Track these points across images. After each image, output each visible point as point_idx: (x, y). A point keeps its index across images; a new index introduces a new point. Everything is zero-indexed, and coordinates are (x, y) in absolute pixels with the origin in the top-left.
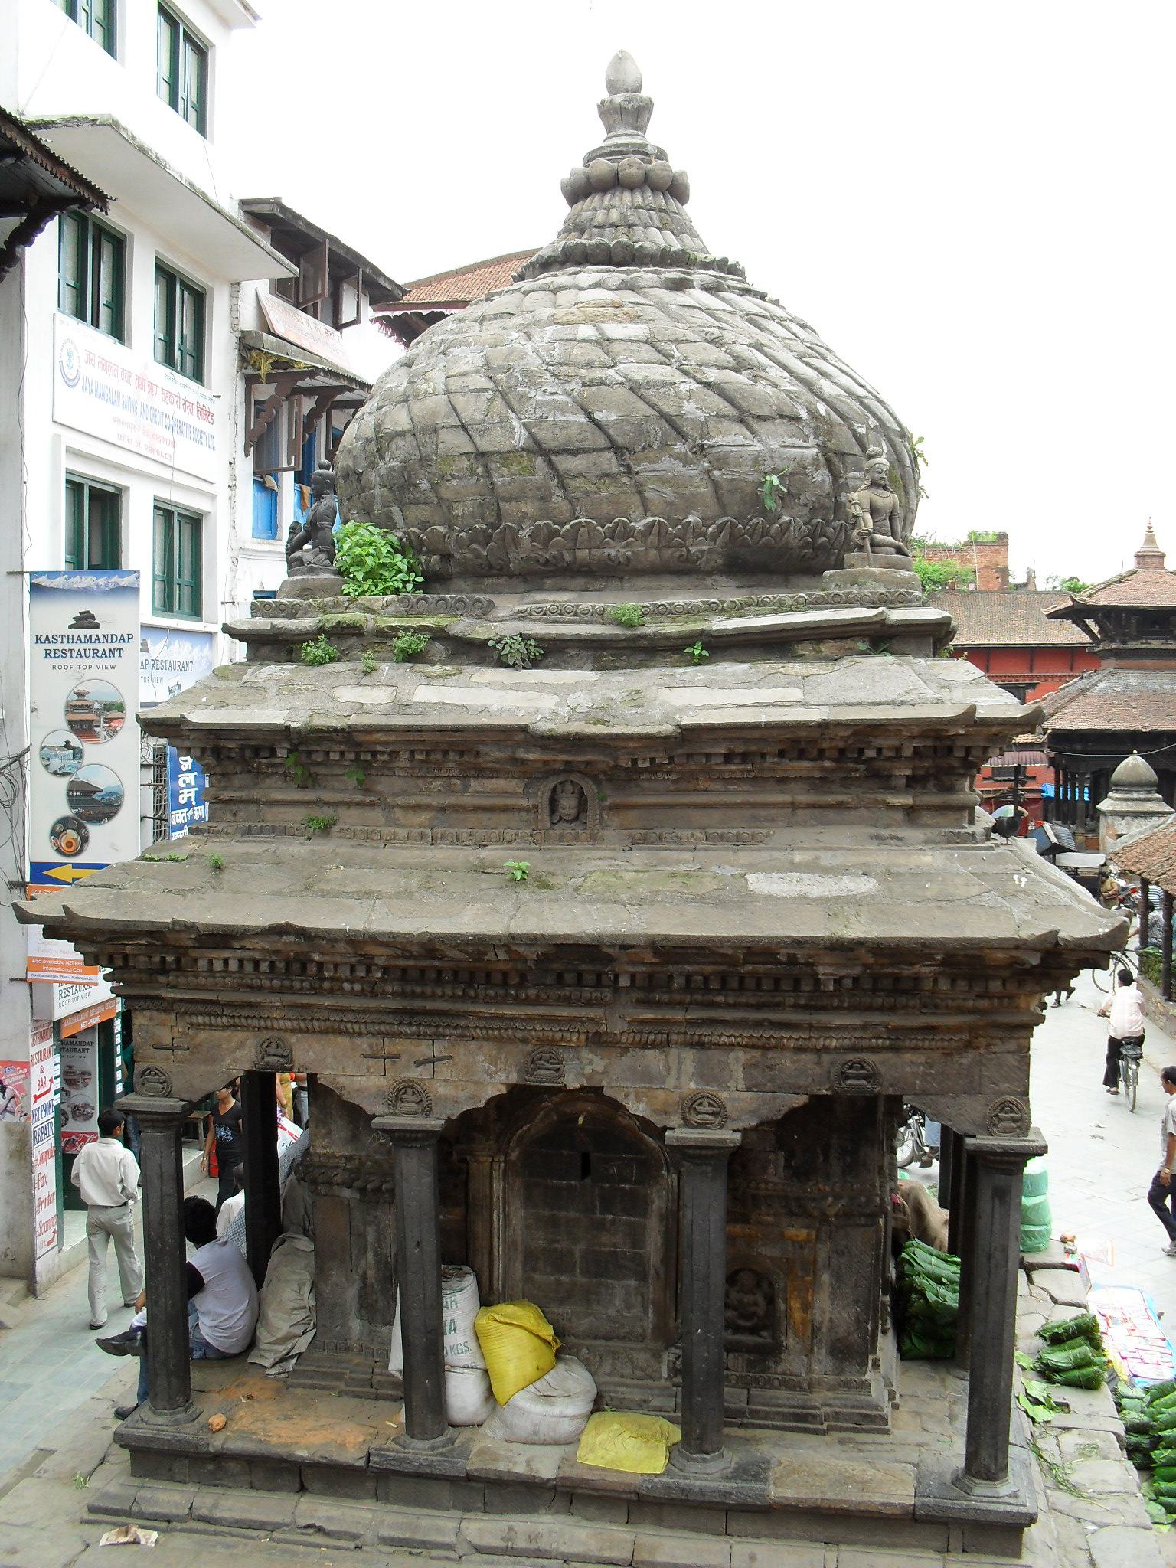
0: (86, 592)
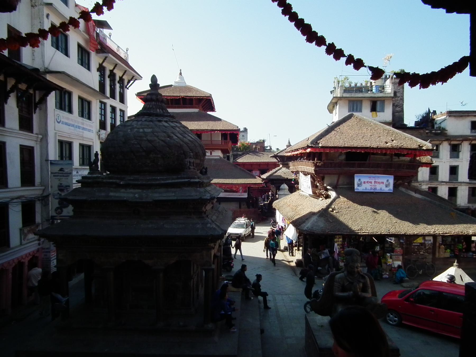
0: (62, 164)
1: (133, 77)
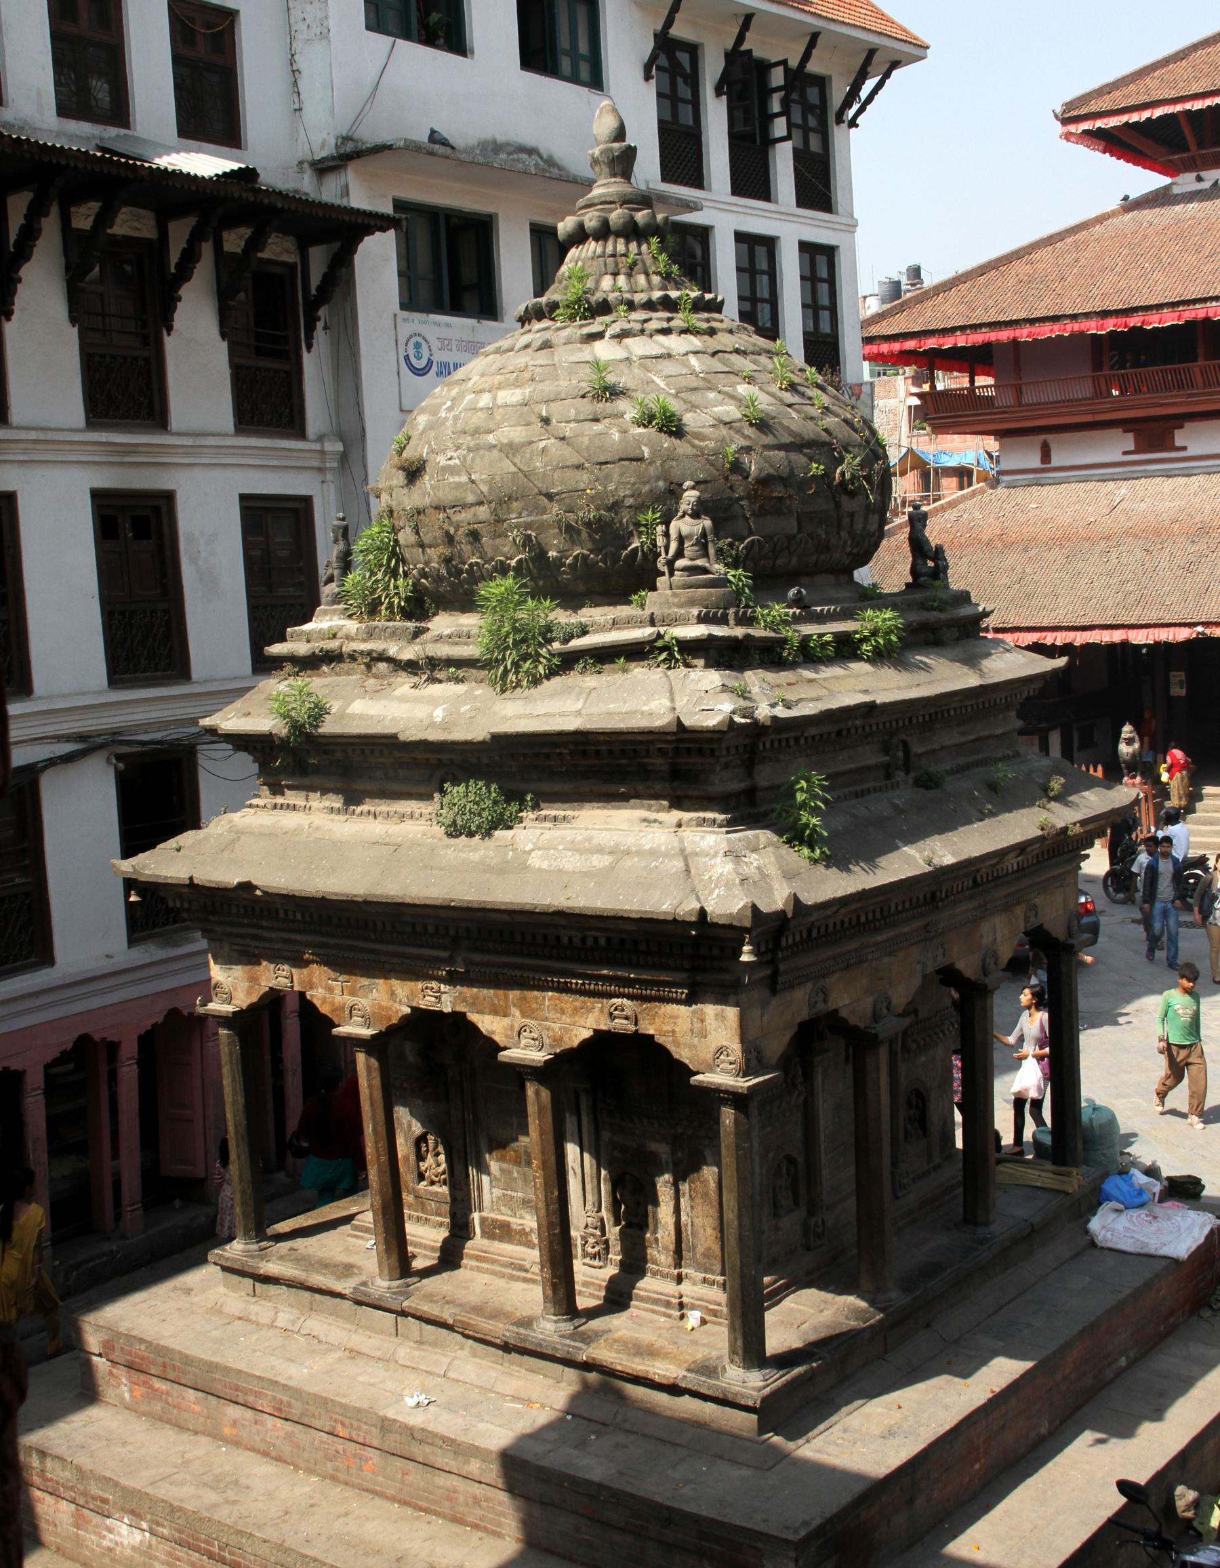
1: (872, 52)
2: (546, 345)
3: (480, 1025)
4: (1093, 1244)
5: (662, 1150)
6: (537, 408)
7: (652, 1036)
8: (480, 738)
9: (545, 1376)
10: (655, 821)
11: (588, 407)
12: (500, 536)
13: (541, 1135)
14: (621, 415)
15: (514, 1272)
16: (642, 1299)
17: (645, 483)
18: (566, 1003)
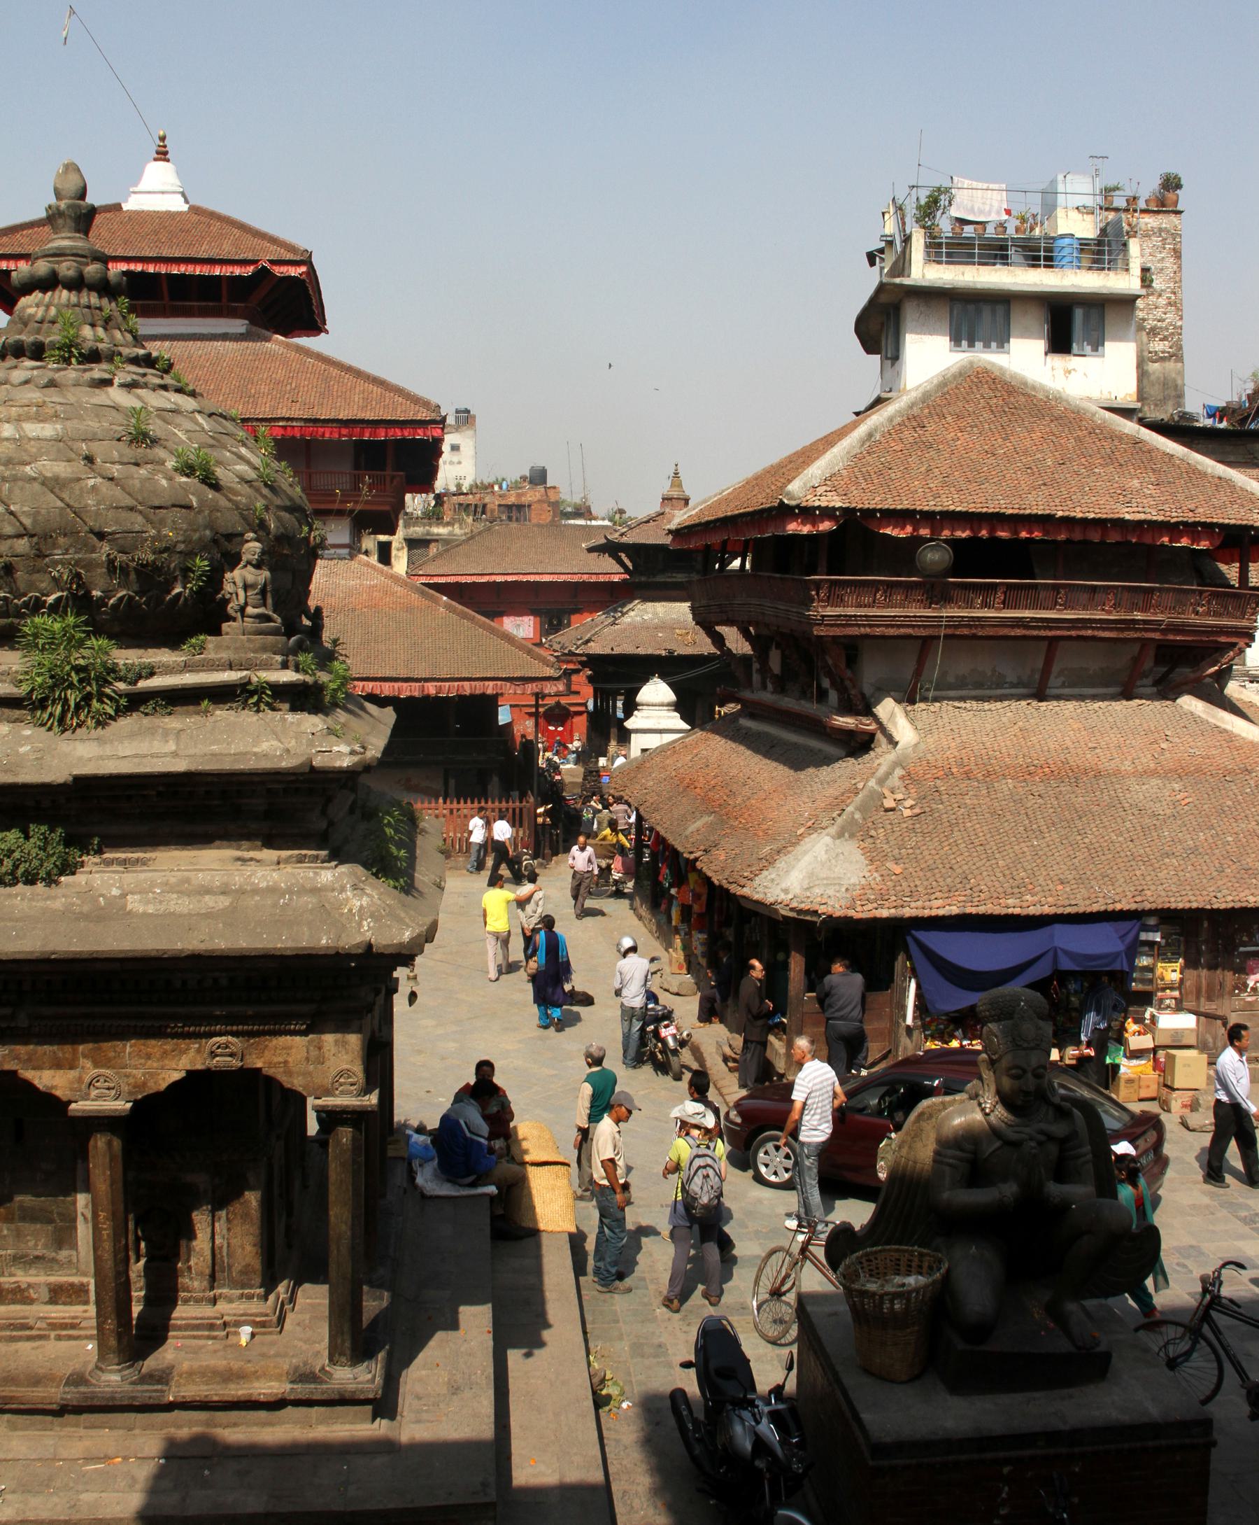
2: (52, 384)
3: (36, 1082)
4: (423, 1196)
5: (201, 1180)
6: (76, 445)
7: (259, 1070)
8: (61, 780)
9: (110, 1428)
10: (251, 859)
11: (130, 453)
12: (38, 572)
13: (112, 1185)
14: (162, 463)
15: (15, 1333)
16: (179, 1328)
17: (195, 531)
18: (154, 1047)
